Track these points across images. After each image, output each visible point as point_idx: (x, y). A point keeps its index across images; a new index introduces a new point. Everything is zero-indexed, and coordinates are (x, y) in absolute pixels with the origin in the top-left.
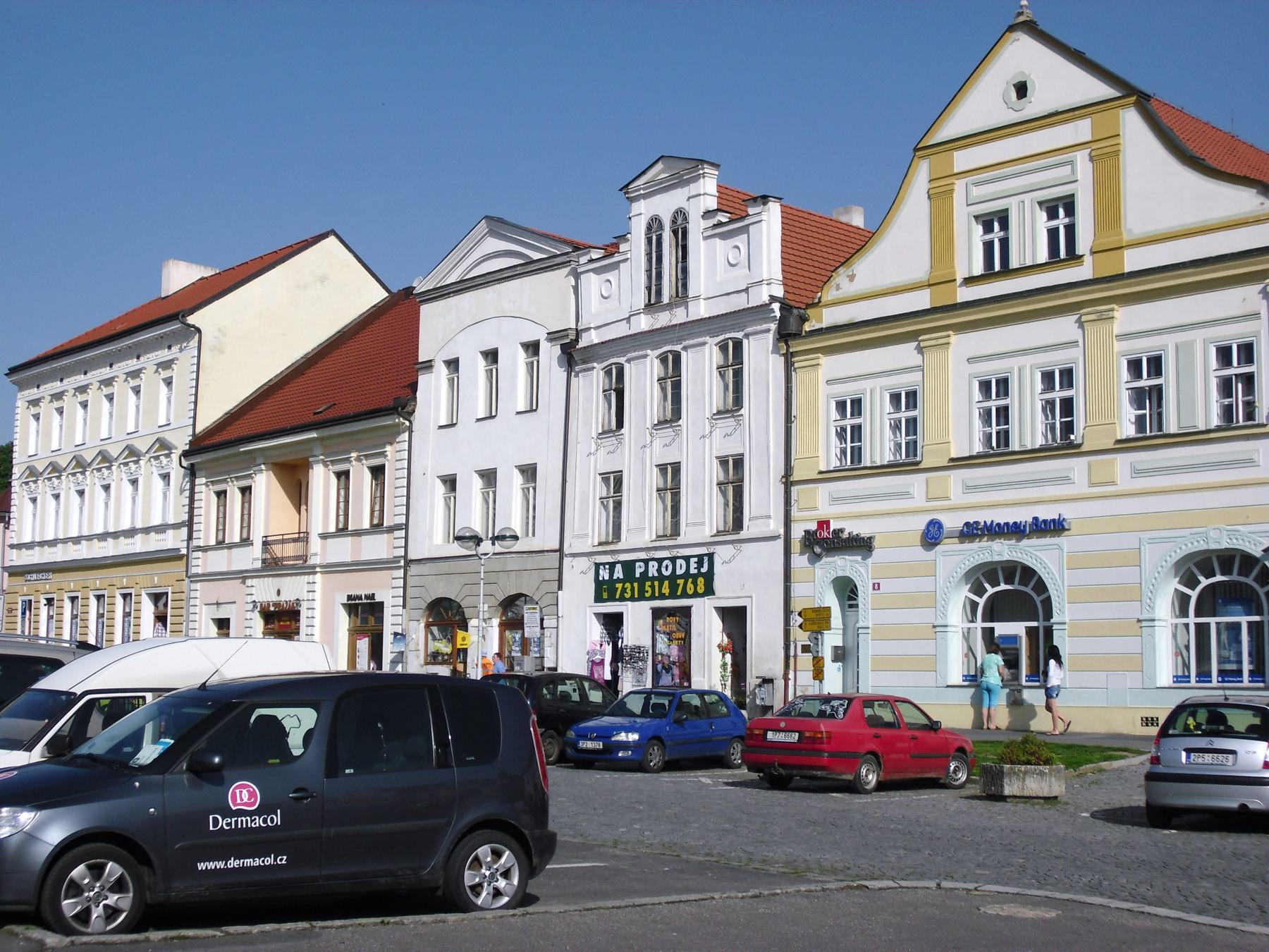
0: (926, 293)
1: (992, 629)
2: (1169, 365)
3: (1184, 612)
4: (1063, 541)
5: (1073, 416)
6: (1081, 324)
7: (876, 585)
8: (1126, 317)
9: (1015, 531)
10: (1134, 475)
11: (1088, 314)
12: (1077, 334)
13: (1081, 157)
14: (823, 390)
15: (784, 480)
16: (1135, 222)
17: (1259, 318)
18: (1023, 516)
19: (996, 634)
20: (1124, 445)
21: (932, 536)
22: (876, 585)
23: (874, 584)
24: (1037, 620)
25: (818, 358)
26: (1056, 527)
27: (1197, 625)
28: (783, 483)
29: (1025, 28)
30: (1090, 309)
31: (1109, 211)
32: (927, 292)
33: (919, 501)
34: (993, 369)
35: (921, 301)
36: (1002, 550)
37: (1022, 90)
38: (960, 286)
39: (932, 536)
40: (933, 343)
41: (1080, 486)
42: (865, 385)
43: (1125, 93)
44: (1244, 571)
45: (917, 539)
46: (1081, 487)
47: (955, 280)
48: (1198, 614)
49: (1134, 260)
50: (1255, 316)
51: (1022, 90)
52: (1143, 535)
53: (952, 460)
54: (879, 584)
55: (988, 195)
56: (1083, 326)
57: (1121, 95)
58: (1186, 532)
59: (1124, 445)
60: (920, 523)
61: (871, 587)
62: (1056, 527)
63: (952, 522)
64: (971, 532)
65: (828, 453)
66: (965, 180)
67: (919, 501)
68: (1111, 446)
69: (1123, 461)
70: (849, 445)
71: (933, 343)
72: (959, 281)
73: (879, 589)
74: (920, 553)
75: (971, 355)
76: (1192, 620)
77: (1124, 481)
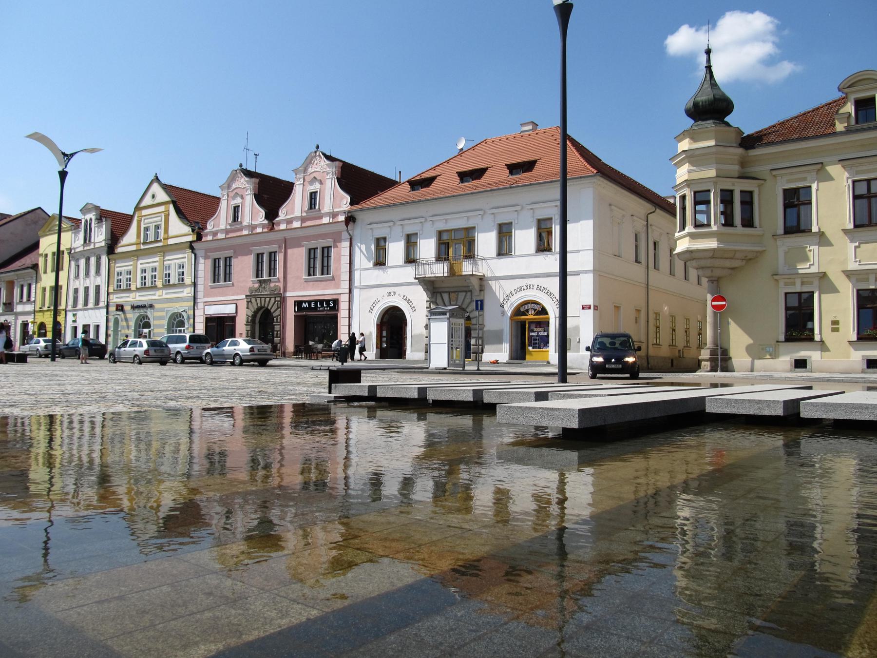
16: (172, 231)
31: (166, 230)
32: (135, 246)
37: (153, 196)
49: (171, 242)
51: (153, 196)
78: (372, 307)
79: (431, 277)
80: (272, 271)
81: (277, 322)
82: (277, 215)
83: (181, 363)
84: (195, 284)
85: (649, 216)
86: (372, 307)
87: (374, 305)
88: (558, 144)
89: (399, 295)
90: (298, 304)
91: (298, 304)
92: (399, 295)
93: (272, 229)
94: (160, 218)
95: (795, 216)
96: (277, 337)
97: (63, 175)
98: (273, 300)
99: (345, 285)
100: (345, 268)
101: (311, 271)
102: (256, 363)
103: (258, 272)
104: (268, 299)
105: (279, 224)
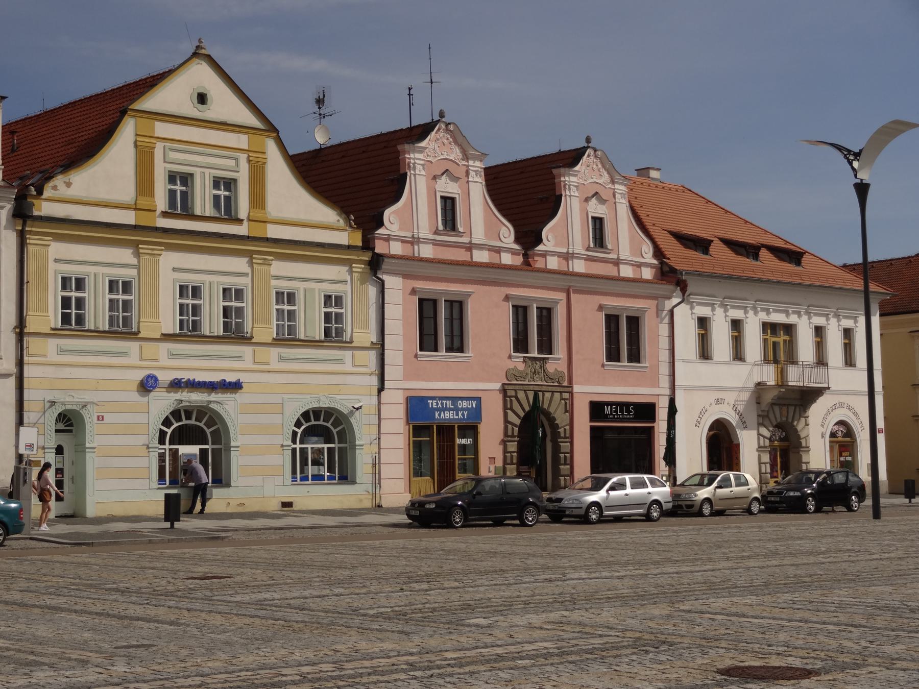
0: (132, 214)
1: (177, 450)
2: (248, 294)
3: (162, 441)
4: (239, 396)
5: (62, 312)
6: (251, 264)
7: (101, 418)
8: (279, 267)
9: (211, 387)
10: (59, 353)
11: (257, 259)
12: (248, 270)
13: (243, 157)
14: (52, 266)
15: (18, 330)
17: (248, 276)
18: (215, 377)
19: (180, 453)
20: (167, 337)
21: (147, 386)
22: (101, 418)
23: (98, 417)
24: (334, 443)
25: (272, 260)
26: (236, 386)
27: (300, 448)
28: (16, 333)
29: (206, 59)
30: (259, 256)
31: (258, 199)
32: (133, 213)
33: (134, 360)
34: (191, 279)
35: (128, 218)
36: (196, 398)
38: (159, 217)
39: (147, 386)
40: (149, 252)
41: (248, 364)
42: (91, 269)
43: (267, 128)
44: (317, 418)
45: (135, 386)
46: (248, 364)
47: (155, 211)
48: (301, 443)
49: (273, 232)
50: (345, 282)
52: (286, 397)
53: (163, 335)
54: (103, 417)
55: (182, 161)
56: (139, 256)
57: (264, 128)
58: (308, 396)
59: (167, 337)
60: (140, 375)
61: (95, 418)
62: (236, 386)
63: (165, 377)
64: (176, 385)
65: (53, 317)
66: (163, 144)
67: (134, 360)
68: (270, 342)
69: (53, 343)
70: (74, 311)
71: (149, 252)
72: (158, 212)
73: (103, 420)
74: (135, 396)
75: (176, 266)
76: (167, 446)
77: (275, 365)
78: (699, 419)
79: (794, 386)
80: (546, 345)
81: (565, 437)
82: (539, 241)
83: (462, 526)
84: (380, 347)
85: (675, 310)
86: (699, 420)
87: (701, 416)
88: (202, 98)
89: (728, 403)
90: (597, 409)
91: (597, 409)
92: (728, 403)
93: (527, 263)
94: (232, 163)
95: (257, 265)
96: (565, 464)
97: (862, 190)
98: (557, 395)
99: (665, 382)
100: (664, 356)
101: (613, 355)
102: (624, 518)
103: (521, 344)
104: (548, 395)
105: (544, 255)
